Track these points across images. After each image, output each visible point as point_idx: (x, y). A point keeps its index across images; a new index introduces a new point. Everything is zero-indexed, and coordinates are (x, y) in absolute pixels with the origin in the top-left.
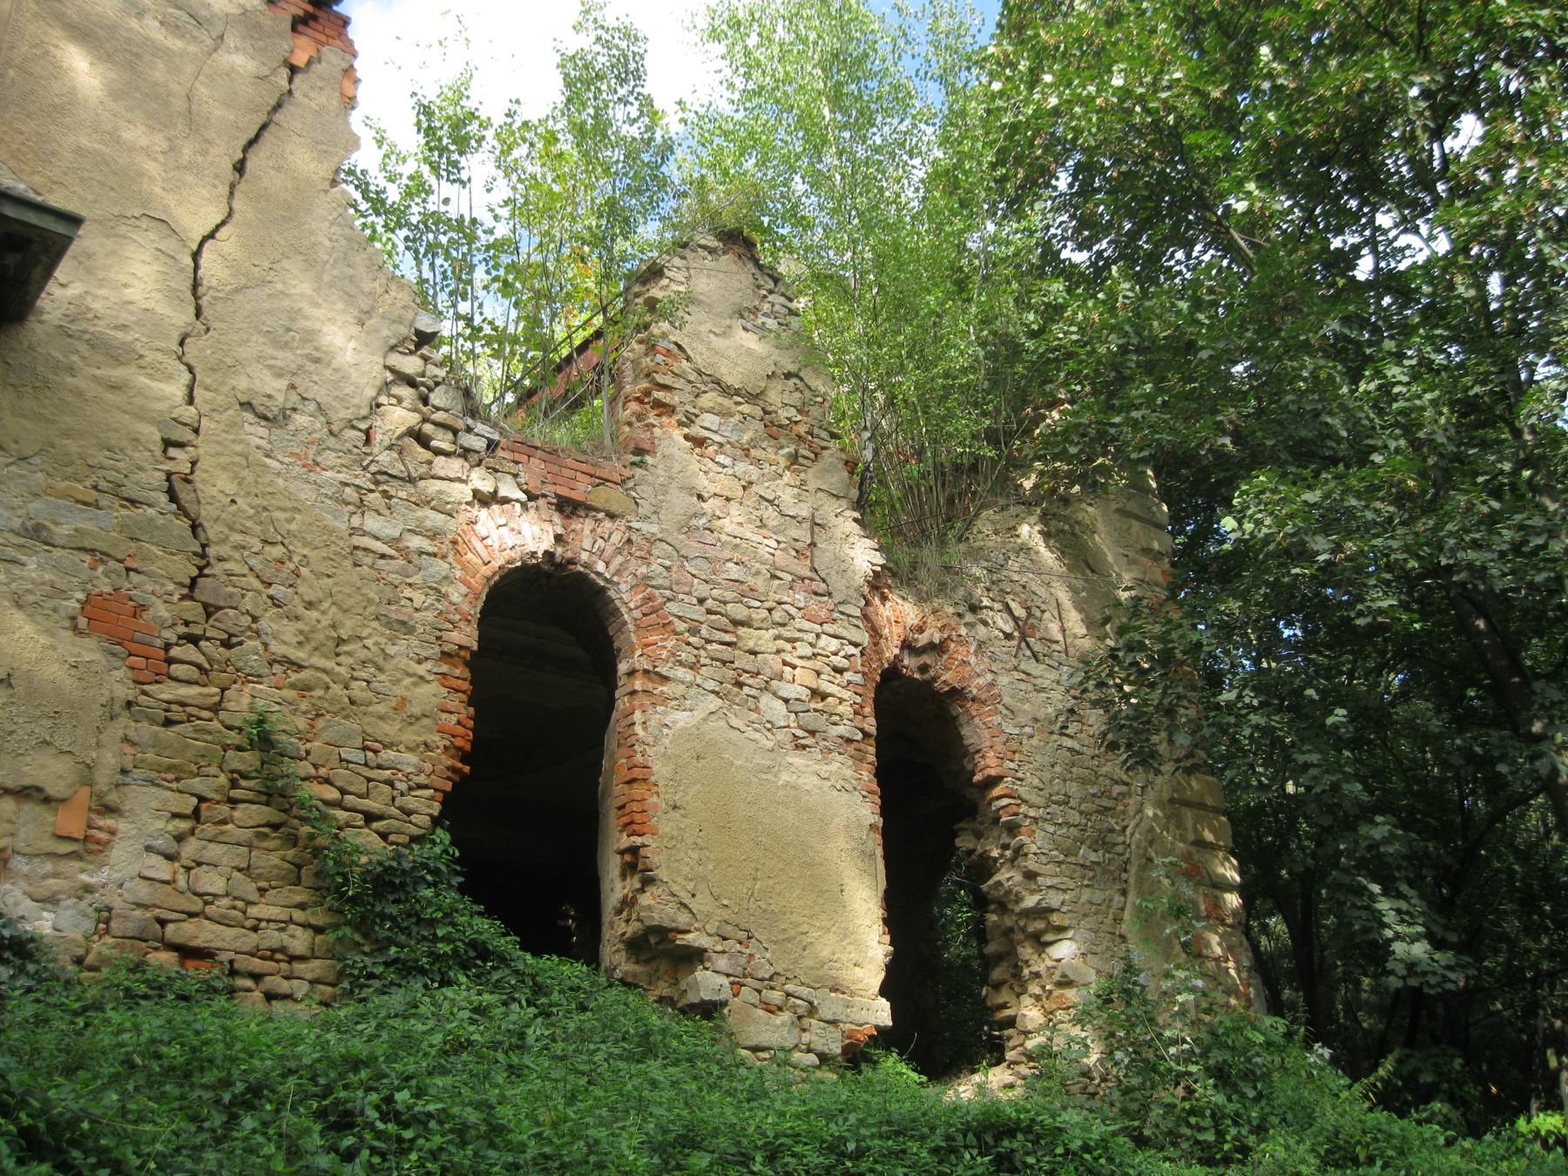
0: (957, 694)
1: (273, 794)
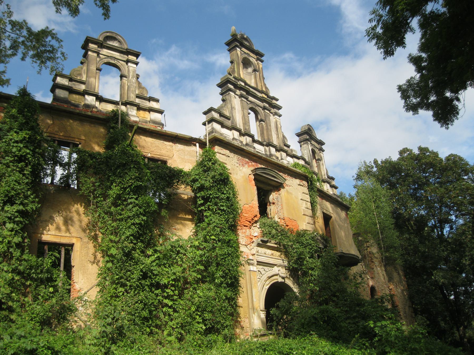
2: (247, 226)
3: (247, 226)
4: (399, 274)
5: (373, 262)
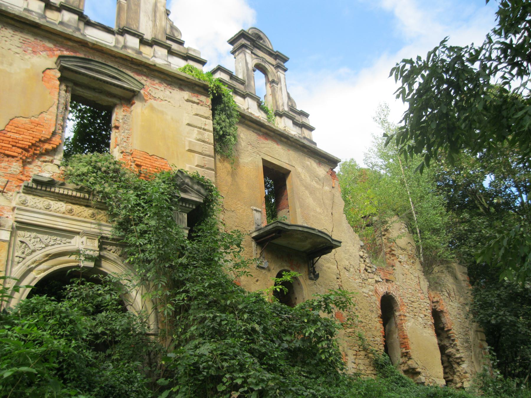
0: (442, 311)
1: (365, 349)
2: (13, 157)
3: (13, 157)
4: (456, 278)
5: (393, 255)
